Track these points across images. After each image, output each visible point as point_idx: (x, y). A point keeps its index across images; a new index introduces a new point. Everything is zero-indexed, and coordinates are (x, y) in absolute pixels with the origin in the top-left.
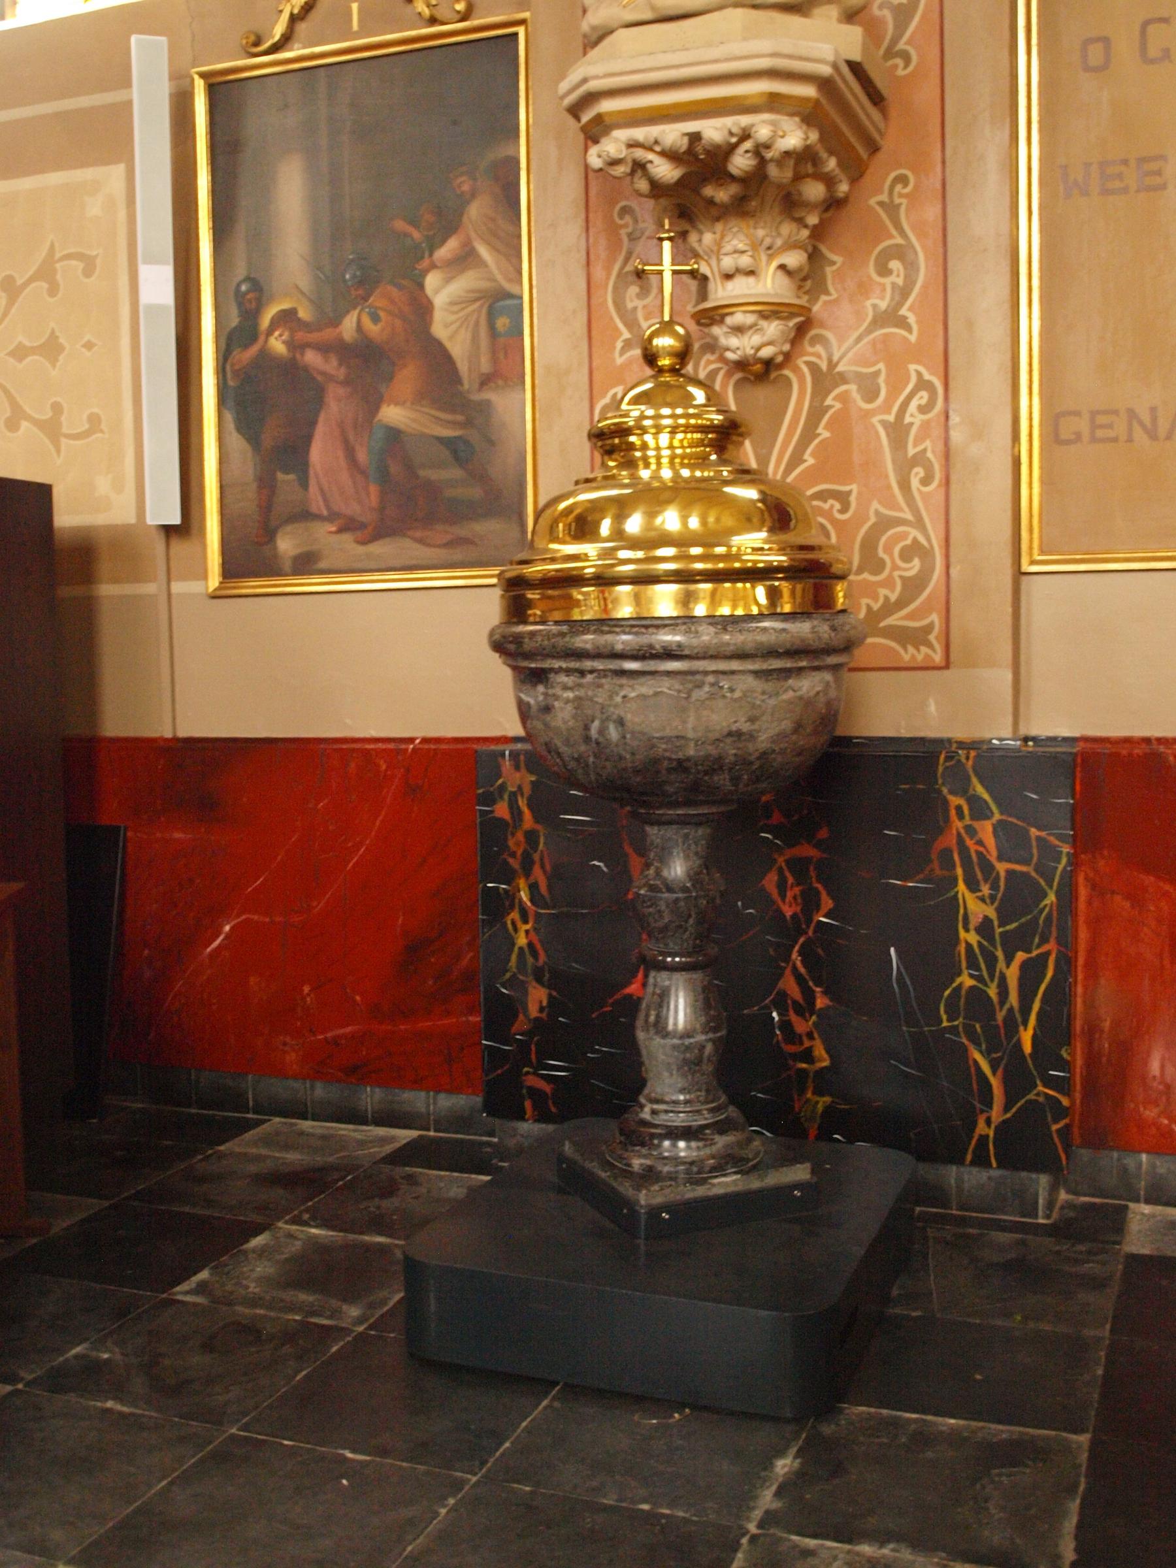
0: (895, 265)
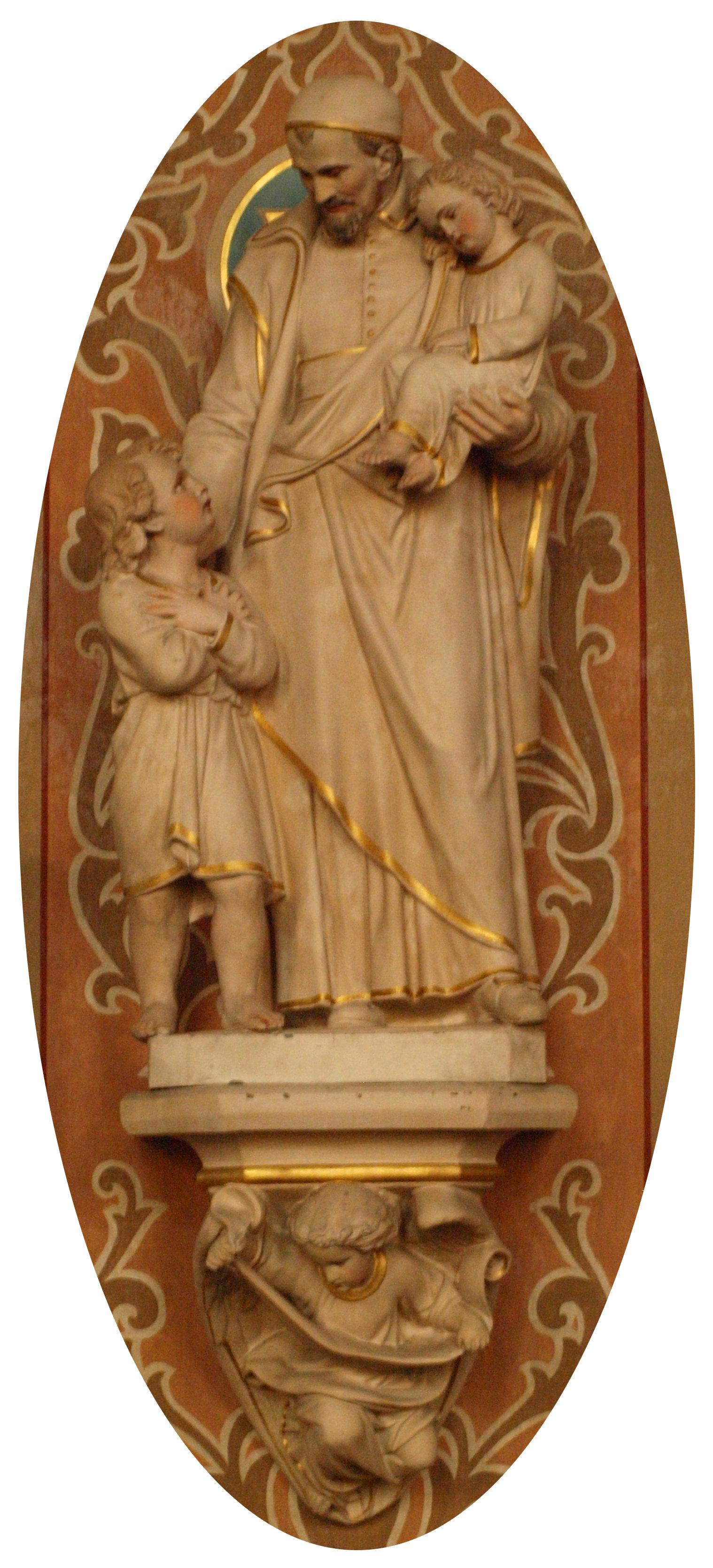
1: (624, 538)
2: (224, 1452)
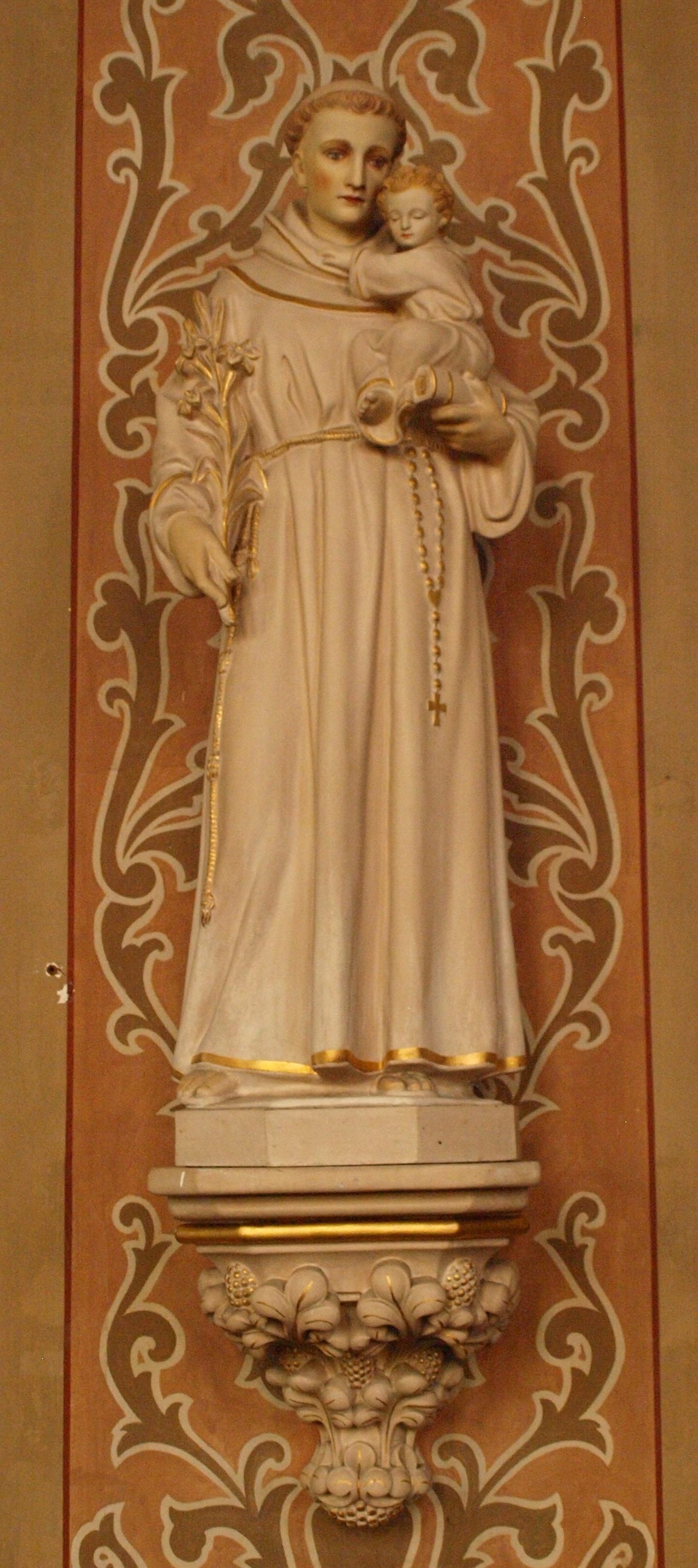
0: (576, 1339)
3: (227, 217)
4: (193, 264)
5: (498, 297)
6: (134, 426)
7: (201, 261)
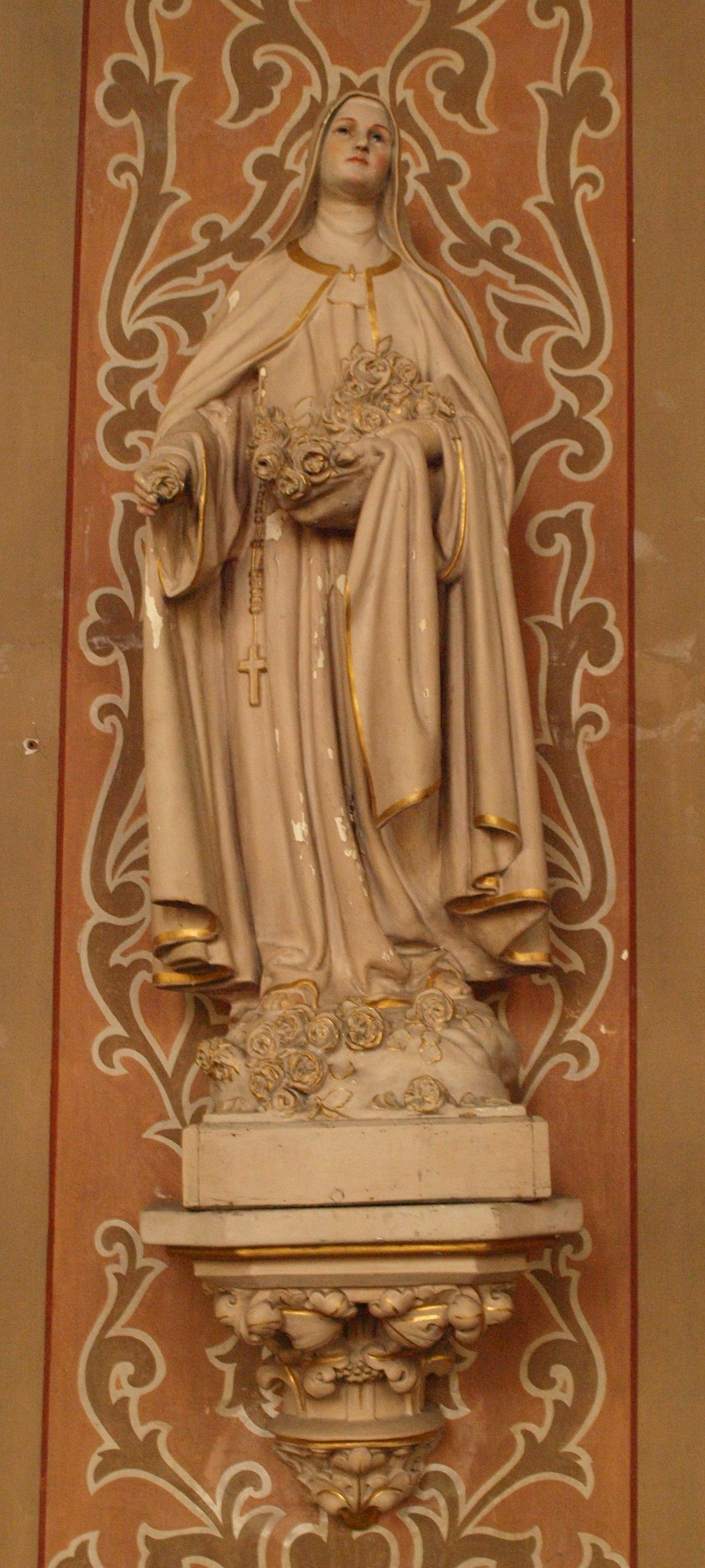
0: (561, 1373)
1: (615, 91)
2: (217, 1509)
3: (229, 228)
4: (193, 274)
5: (502, 320)
6: (132, 439)
7: (201, 271)
